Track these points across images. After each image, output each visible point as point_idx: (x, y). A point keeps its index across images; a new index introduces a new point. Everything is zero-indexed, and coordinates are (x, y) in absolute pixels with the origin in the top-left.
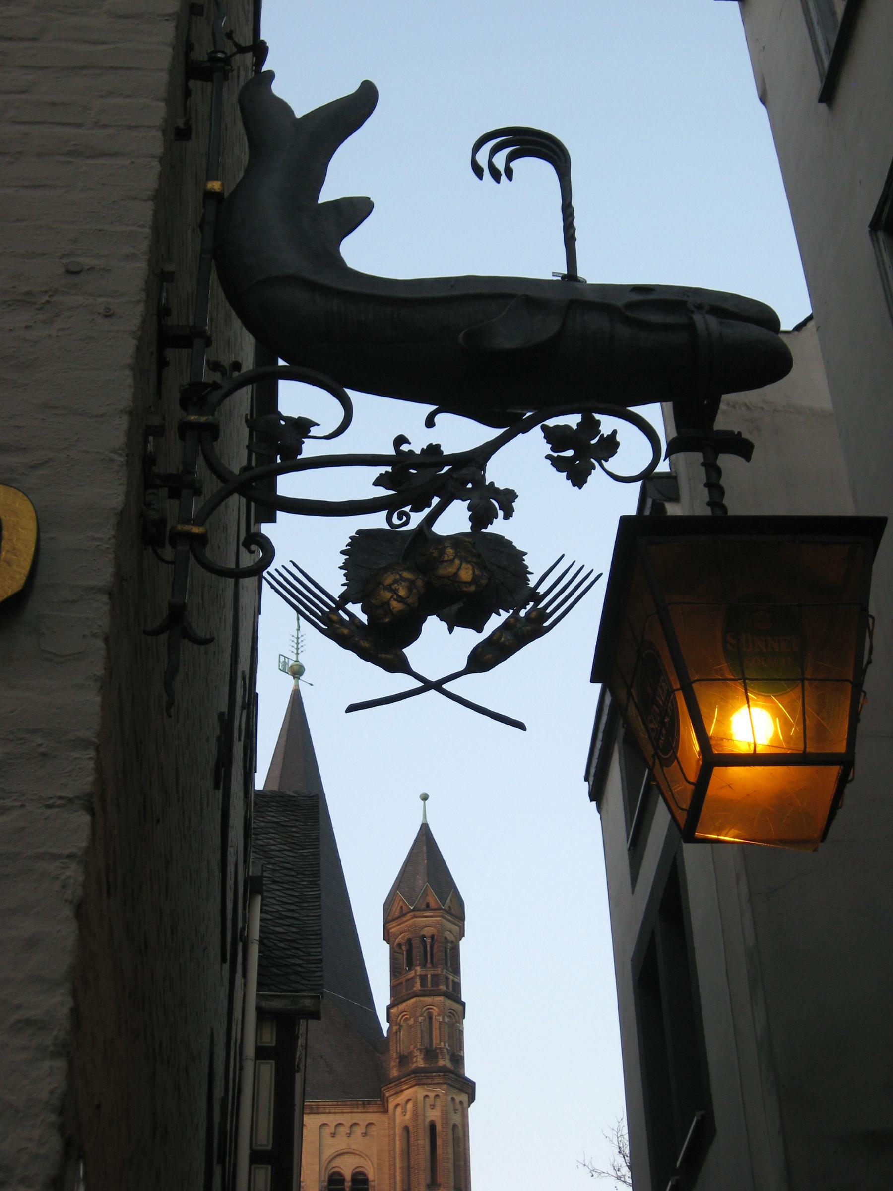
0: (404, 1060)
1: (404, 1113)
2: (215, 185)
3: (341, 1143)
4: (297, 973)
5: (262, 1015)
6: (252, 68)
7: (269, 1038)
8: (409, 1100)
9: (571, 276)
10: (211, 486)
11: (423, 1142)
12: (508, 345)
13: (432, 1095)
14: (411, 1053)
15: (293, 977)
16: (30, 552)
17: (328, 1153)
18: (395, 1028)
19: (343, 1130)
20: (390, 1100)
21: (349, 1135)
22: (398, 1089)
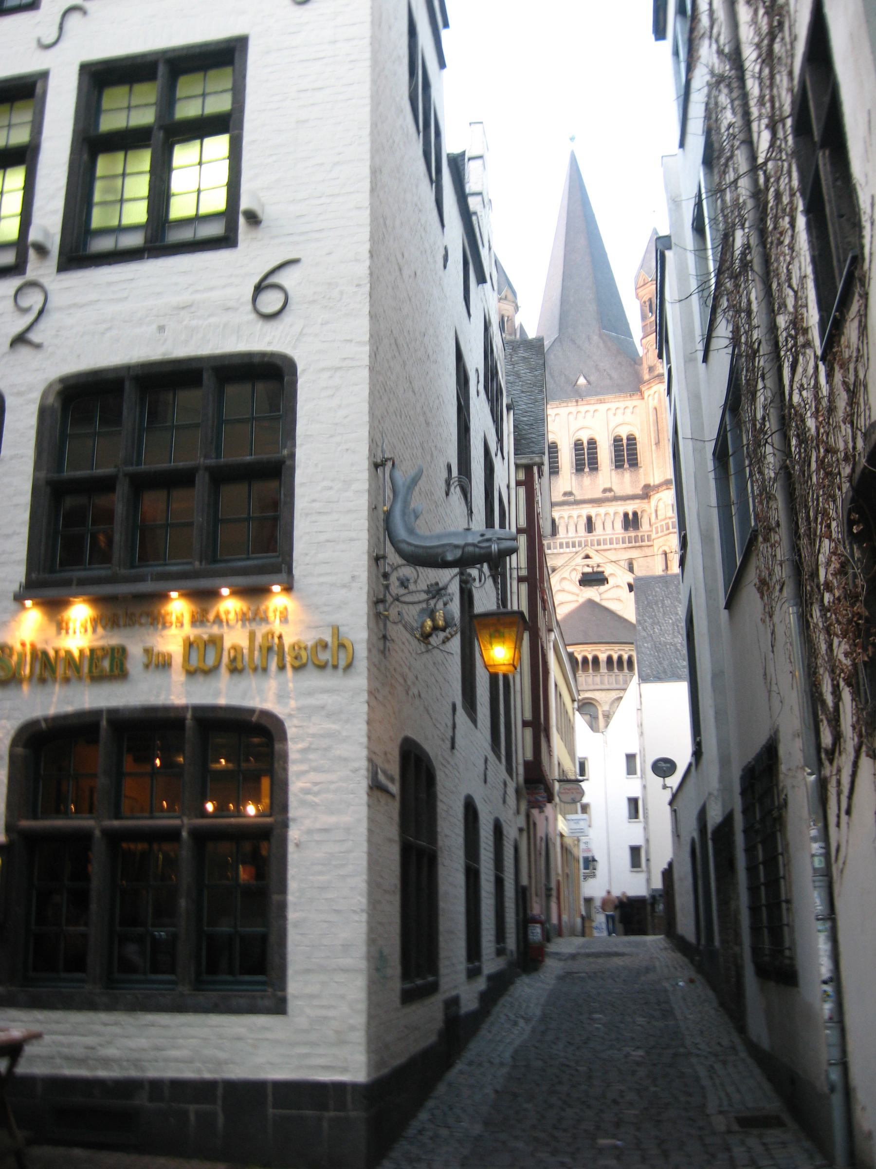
1: (653, 399)
2: (385, 508)
3: (619, 419)
4: (533, 442)
5: (517, 466)
7: (522, 476)
8: (655, 393)
14: (655, 365)
15: (531, 445)
16: (172, 697)
17: (611, 427)
18: (645, 351)
19: (620, 412)
20: (645, 392)
21: (624, 413)
22: (649, 386)
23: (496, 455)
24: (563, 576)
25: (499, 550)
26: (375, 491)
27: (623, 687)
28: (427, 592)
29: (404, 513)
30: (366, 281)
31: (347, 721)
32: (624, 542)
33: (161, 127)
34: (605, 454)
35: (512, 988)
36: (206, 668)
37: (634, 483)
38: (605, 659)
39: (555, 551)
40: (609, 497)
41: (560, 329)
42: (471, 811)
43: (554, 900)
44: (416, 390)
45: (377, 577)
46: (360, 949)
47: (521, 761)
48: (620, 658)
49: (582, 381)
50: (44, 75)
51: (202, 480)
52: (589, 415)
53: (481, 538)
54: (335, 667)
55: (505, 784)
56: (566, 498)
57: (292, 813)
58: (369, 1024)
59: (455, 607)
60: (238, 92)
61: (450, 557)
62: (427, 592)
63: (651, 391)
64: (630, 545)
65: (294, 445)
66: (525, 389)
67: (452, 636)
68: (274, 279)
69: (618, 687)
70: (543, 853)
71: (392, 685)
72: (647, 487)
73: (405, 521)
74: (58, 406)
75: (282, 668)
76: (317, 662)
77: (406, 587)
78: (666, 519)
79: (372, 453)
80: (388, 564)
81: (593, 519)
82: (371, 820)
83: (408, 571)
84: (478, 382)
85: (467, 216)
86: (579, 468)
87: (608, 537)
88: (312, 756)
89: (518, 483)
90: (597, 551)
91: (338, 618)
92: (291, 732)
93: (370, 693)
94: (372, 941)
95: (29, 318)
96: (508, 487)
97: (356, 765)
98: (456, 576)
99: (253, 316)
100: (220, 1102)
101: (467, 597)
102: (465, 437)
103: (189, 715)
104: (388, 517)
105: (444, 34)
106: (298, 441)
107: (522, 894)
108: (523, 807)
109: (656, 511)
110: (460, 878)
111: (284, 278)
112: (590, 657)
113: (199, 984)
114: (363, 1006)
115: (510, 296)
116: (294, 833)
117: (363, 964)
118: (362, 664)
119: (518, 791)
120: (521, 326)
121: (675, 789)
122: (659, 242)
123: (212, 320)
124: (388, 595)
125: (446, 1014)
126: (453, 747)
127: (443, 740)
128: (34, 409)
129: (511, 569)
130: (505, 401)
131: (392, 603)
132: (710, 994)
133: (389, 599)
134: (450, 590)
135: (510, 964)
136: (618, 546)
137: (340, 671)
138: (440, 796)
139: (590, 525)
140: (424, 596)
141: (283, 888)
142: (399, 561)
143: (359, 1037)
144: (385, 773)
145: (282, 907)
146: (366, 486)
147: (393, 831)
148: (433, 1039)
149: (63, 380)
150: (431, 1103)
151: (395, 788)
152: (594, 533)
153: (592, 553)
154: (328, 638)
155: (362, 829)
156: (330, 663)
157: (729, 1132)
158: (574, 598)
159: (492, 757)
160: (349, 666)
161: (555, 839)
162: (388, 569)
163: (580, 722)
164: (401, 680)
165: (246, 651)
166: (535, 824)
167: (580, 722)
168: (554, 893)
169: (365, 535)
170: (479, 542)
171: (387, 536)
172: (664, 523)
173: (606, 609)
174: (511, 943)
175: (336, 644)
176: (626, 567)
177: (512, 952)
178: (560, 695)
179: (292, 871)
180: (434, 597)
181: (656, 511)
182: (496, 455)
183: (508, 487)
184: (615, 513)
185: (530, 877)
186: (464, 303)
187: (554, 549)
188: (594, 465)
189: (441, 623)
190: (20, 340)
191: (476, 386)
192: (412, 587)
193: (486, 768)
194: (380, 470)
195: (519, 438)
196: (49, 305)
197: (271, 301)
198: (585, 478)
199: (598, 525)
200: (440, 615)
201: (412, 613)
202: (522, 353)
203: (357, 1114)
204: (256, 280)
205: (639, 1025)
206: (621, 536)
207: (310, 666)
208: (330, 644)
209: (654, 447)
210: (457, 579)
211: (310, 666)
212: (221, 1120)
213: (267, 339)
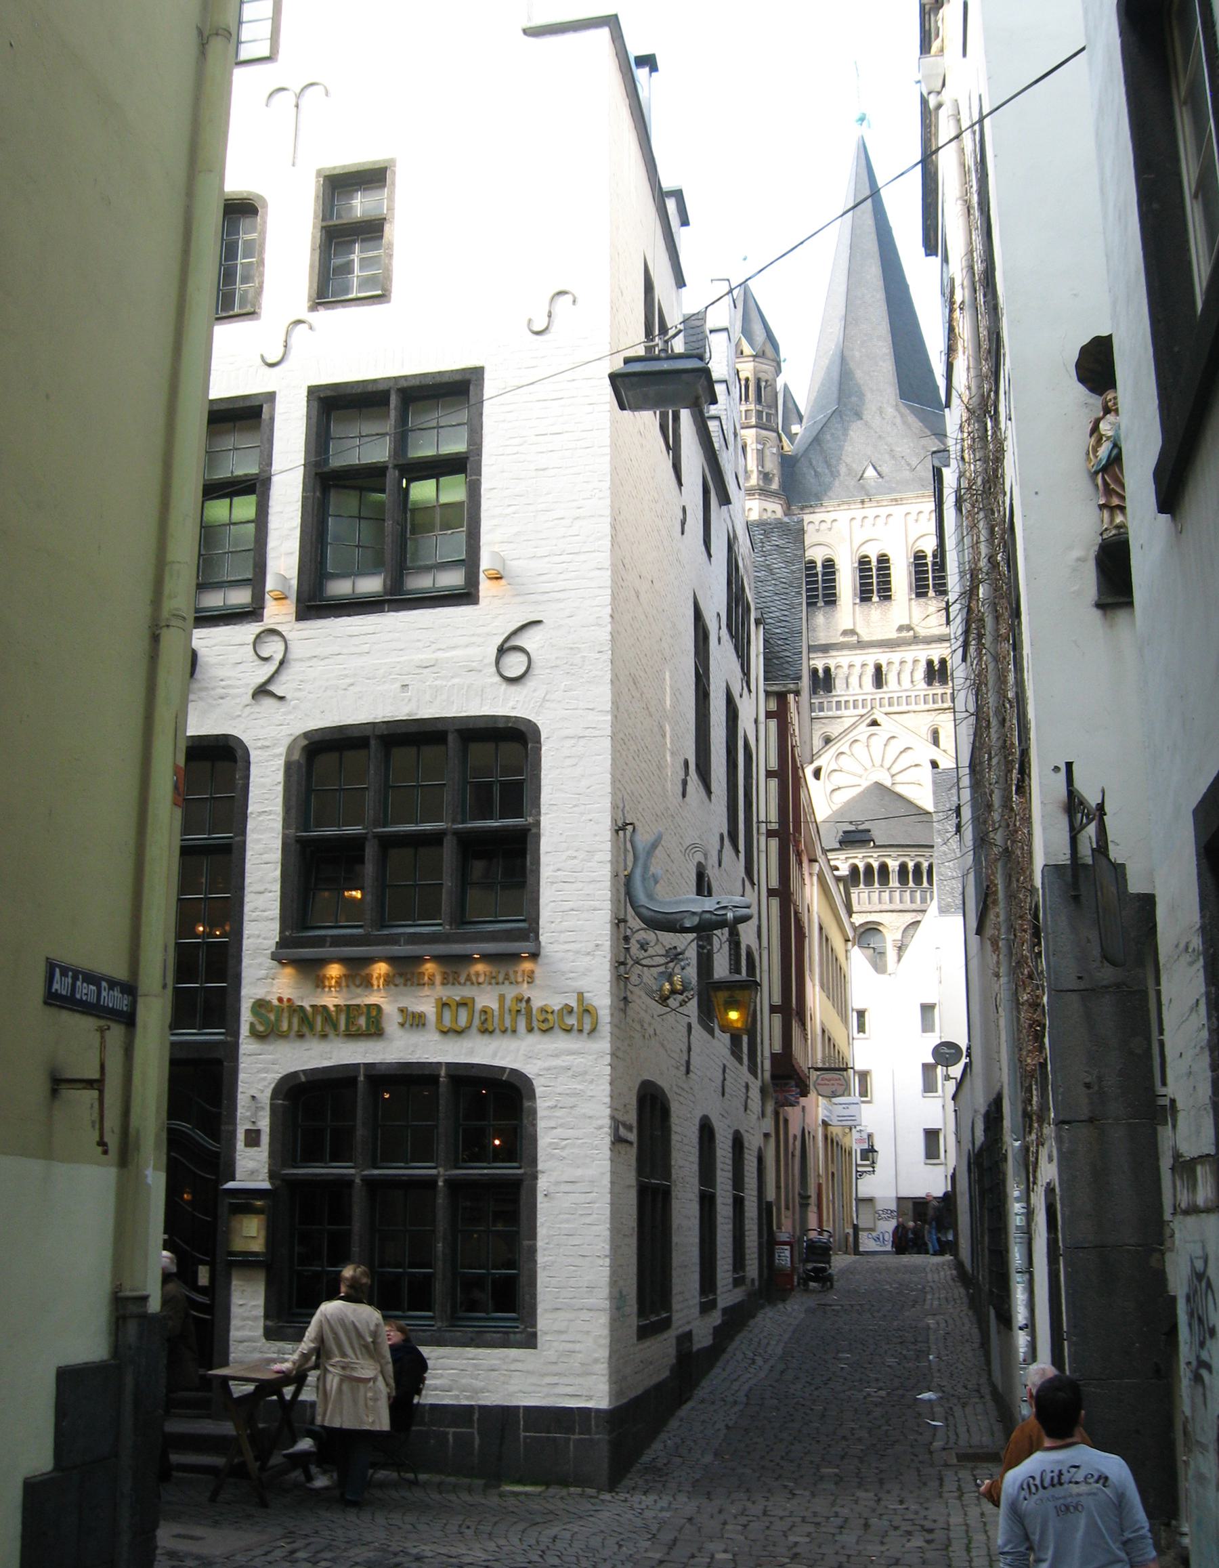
2: (626, 873)
4: (788, 662)
5: (767, 694)
6: (813, 1291)
7: (773, 706)
9: (242, 43)
15: (786, 666)
23: (741, 696)
24: (839, 751)
27: (923, 907)
29: (644, 879)
30: (607, 647)
31: (592, 1082)
33: (396, 466)
35: (752, 1323)
36: (459, 1029)
38: (897, 869)
39: (830, 714)
41: (839, 399)
42: (706, 1131)
43: (812, 1209)
45: (618, 939)
46: (604, 1291)
47: (767, 1054)
49: (870, 473)
50: (271, 397)
52: (880, 521)
54: (580, 1031)
55: (747, 1087)
56: (846, 639)
57: (540, 1166)
58: (610, 1357)
59: (692, 972)
64: (936, 706)
65: (539, 813)
66: (779, 589)
67: (690, 999)
68: (518, 641)
69: (914, 907)
70: (798, 1153)
73: (645, 888)
74: (303, 761)
77: (646, 951)
79: (614, 821)
81: (884, 669)
82: (613, 1173)
83: (650, 936)
84: (720, 628)
86: (864, 595)
87: (904, 694)
88: (559, 1113)
89: (769, 715)
92: (539, 1091)
93: (613, 1054)
94: (614, 1283)
95: (271, 668)
96: (756, 721)
97: (600, 1122)
98: (693, 941)
99: (497, 679)
100: (476, 1425)
101: (705, 962)
102: (704, 703)
103: (443, 1073)
104: (629, 879)
105: (683, 236)
106: (543, 810)
107: (766, 1211)
108: (770, 1108)
110: (694, 1209)
111: (528, 641)
112: (876, 865)
113: (454, 1320)
114: (606, 1342)
115: (769, 351)
116: (542, 1184)
117: (606, 1304)
118: (605, 1028)
119: (763, 1091)
120: (786, 387)
121: (959, 1077)
123: (456, 681)
125: (678, 1351)
126: (688, 1072)
127: (677, 1068)
128: (281, 762)
129: (758, 822)
130: (753, 615)
131: (632, 966)
133: (630, 962)
134: (687, 954)
135: (749, 1295)
138: (674, 1128)
139: (879, 678)
140: (662, 960)
141: (533, 1235)
143: (602, 1368)
144: (624, 1125)
145: (533, 1251)
146: (608, 857)
147: (631, 1178)
148: (666, 1374)
149: (306, 735)
150: (663, 1436)
151: (633, 1137)
152: (885, 689)
153: (880, 718)
154: (574, 1004)
155: (606, 1181)
156: (575, 1027)
158: (856, 781)
159: (731, 1062)
160: (593, 1030)
161: (816, 1131)
162: (629, 932)
163: (857, 962)
164: (638, 1027)
165: (496, 1013)
166: (786, 1121)
167: (857, 962)
168: (813, 1200)
169: (607, 905)
170: (716, 910)
171: (628, 904)
173: (900, 797)
174: (752, 1270)
177: (753, 1280)
178: (827, 939)
179: (541, 1219)
182: (741, 696)
183: (756, 721)
184: (915, 661)
185: (778, 1187)
186: (703, 548)
187: (828, 710)
188: (886, 594)
190: (262, 691)
192: (651, 951)
193: (724, 1079)
195: (770, 656)
196: (291, 656)
197: (514, 665)
198: (873, 611)
199: (891, 678)
201: (649, 976)
202: (776, 540)
203: (601, 1437)
205: (889, 1366)
206: (922, 693)
208: (575, 1009)
210: (694, 945)
211: (557, 1029)
212: (477, 1442)
213: (511, 704)
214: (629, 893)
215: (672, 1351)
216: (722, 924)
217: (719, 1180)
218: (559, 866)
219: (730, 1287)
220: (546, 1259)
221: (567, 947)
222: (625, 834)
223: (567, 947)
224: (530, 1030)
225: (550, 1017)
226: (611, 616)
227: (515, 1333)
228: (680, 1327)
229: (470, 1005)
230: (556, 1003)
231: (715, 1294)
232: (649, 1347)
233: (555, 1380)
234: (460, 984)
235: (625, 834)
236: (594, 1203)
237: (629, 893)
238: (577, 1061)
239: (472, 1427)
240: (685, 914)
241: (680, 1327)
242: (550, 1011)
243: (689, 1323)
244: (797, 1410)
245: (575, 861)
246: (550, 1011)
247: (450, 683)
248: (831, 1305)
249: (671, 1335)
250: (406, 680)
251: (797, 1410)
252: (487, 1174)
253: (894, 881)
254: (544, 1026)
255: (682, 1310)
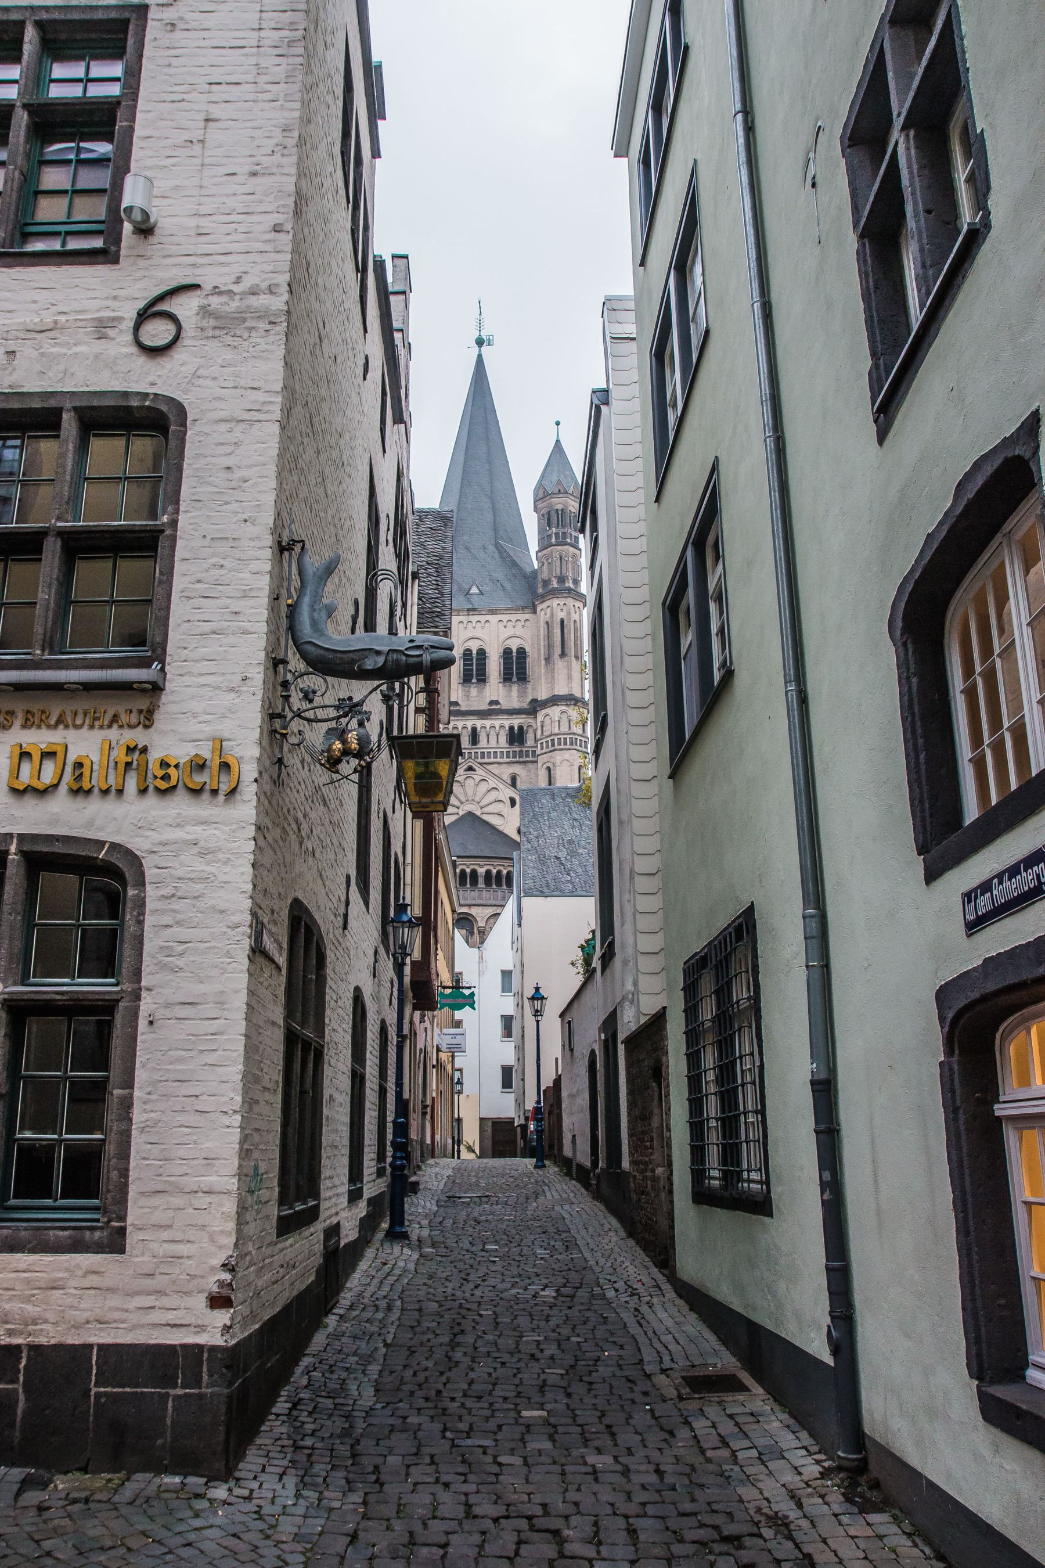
0: (546, 583)
2: (290, 601)
3: (510, 631)
10: (290, 715)
11: (557, 631)
12: (369, 668)
13: (562, 603)
17: (501, 639)
25: (432, 661)
26: (279, 579)
27: (502, 903)
28: (337, 708)
31: (227, 862)
32: (508, 757)
34: (494, 666)
36: (40, 787)
37: (522, 695)
40: (493, 711)
44: (329, 493)
48: (499, 872)
51: (52, 549)
53: (410, 645)
60: (132, 79)
61: (369, 664)
62: (337, 708)
63: (544, 605)
71: (284, 829)
72: (534, 701)
75: (143, 791)
76: (191, 786)
77: (311, 701)
78: (552, 735)
79: (276, 530)
80: (290, 671)
83: (314, 681)
85: (388, 331)
86: (467, 679)
88: (176, 905)
90: (481, 764)
91: (225, 728)
97: (235, 919)
99: (134, 349)
104: (293, 610)
107: (403, 1108)
109: (542, 726)
116: (146, 1005)
118: (249, 791)
122: (594, 396)
124: (287, 709)
125: (325, 1247)
126: (345, 927)
127: (335, 915)
132: (614, 1222)
136: (501, 760)
137: (221, 798)
140: (332, 713)
142: (302, 666)
157: (681, 1398)
159: (382, 951)
162: (289, 677)
163: (459, 936)
164: (294, 826)
170: (407, 649)
172: (549, 739)
175: (217, 761)
176: (509, 781)
180: (345, 715)
181: (542, 726)
188: (482, 678)
189: (354, 746)
191: (386, 534)
192: (318, 701)
193: (376, 961)
194: (286, 554)
197: (157, 332)
200: (352, 737)
201: (316, 736)
203: (211, 1387)
204: (141, 304)
205: (542, 1259)
207: (181, 788)
209: (543, 662)
211: (181, 790)
214: (292, 628)
215: (319, 1248)
216: (416, 669)
217: (368, 1063)
218: (199, 576)
219: (374, 1176)
220: (146, 1116)
221: (203, 680)
222: (290, 555)
223: (203, 680)
224: (143, 791)
225: (172, 771)
226: (289, 285)
227: (92, 1229)
228: (331, 1216)
229: (60, 755)
230: (182, 753)
231: (362, 1182)
232: (291, 1246)
233: (149, 1301)
234: (49, 727)
235: (290, 555)
236: (222, 1033)
237: (292, 628)
238: (206, 833)
239: (14, 1381)
240: (367, 653)
241: (331, 1216)
242: (173, 764)
243: (337, 1214)
244: (464, 1317)
245: (222, 572)
246: (173, 764)
247: (70, 352)
248: (460, 1198)
249: (318, 1228)
250: (12, 346)
251: (464, 1317)
252: (67, 992)
253: (481, 884)
254: (163, 785)
255: (330, 1198)
